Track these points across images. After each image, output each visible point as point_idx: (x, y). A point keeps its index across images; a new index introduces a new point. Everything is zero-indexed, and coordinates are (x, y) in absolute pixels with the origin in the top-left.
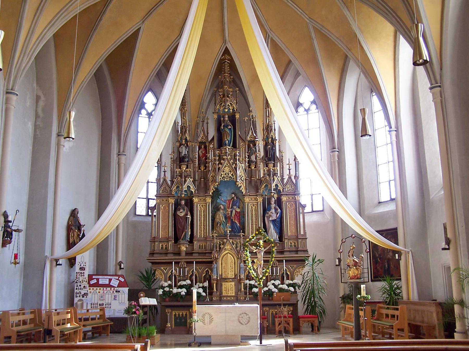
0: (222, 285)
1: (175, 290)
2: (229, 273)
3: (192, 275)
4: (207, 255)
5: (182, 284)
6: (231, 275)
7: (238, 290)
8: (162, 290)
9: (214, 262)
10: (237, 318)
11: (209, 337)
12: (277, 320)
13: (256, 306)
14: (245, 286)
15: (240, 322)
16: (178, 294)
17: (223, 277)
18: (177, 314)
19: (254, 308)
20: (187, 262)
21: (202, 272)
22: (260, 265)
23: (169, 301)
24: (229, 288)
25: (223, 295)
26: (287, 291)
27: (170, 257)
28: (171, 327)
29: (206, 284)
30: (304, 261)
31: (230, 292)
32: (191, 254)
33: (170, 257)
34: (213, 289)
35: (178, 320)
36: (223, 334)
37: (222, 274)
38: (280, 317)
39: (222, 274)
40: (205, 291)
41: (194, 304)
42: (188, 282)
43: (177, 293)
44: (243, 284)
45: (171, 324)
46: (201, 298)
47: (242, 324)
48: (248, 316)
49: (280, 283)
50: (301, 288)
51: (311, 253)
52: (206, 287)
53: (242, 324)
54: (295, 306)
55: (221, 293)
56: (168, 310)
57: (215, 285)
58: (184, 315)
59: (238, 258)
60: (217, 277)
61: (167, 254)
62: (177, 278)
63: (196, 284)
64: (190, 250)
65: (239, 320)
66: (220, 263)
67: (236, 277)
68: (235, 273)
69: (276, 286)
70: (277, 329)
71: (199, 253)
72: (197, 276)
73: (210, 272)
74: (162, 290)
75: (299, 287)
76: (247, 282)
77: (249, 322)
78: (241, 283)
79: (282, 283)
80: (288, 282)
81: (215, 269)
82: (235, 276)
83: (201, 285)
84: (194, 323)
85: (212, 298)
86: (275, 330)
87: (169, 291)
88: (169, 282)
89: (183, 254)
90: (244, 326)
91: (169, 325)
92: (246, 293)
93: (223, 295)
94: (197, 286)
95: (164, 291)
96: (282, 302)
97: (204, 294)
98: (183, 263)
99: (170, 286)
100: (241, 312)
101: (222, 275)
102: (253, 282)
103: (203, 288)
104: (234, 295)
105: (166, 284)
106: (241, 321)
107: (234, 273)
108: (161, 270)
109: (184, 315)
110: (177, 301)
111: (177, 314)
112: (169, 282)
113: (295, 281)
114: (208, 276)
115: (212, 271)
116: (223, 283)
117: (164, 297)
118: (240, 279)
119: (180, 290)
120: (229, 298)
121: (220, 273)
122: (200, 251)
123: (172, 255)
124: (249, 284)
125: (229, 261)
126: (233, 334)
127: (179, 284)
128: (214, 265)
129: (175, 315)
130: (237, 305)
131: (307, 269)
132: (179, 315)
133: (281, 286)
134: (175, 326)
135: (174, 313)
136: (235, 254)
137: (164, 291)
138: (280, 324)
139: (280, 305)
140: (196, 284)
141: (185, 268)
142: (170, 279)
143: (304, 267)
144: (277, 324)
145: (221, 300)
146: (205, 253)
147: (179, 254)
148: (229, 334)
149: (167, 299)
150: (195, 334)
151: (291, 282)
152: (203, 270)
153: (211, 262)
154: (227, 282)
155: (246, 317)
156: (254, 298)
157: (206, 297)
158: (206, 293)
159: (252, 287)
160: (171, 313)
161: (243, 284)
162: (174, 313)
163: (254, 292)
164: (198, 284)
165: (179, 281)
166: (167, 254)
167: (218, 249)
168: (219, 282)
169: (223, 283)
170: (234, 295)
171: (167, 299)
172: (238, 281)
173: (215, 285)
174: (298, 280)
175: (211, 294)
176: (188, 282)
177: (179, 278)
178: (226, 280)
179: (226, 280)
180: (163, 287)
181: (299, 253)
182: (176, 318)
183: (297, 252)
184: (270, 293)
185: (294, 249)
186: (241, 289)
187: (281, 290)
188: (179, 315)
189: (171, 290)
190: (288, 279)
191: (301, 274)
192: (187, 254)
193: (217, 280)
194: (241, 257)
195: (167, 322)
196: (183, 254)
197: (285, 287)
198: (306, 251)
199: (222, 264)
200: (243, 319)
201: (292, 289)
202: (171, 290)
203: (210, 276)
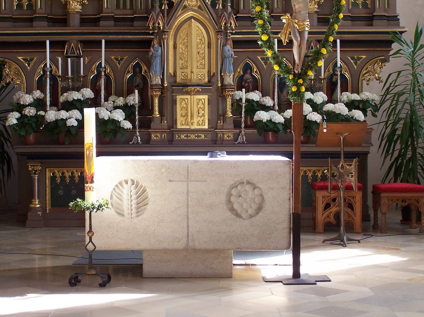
0: (174, 102)
1: (52, 115)
2: (194, 70)
3: (98, 77)
4: (136, 23)
5: (70, 99)
6: (199, 73)
7: (217, 115)
8: (17, 115)
9: (155, 42)
10: (223, 198)
11: (140, 252)
12: (321, 197)
13: (276, 161)
14: (237, 104)
15: (232, 210)
16: (60, 124)
17: (178, 80)
18: (58, 175)
19: (271, 167)
20: (86, 44)
21: (124, 71)
22: (301, 33)
23: (37, 142)
24: (194, 112)
25: (179, 126)
26: (348, 119)
27: (40, 28)
28: (43, 208)
29: (134, 99)
30: (389, 43)
31: (195, 120)
32: (95, 21)
33: (40, 28)
34: (152, 111)
35: (61, 192)
36: (180, 245)
37: (175, 72)
38: (335, 188)
39: (175, 72)
40: (129, 117)
41: (86, 153)
42: (88, 93)
43: (56, 121)
44: (229, 101)
45: (43, 202)
46: (119, 135)
47: (238, 215)
48: (256, 191)
49: (326, 99)
50: (379, 114)
51: (407, 24)
52: (133, 106)
53: (238, 215)
54: (362, 157)
55: (174, 122)
56: (34, 167)
57: (156, 101)
58: (77, 180)
59: (218, 32)
60: (162, 80)
61: (31, 20)
62: (61, 84)
63: (106, 100)
64: (91, 12)
65: (229, 202)
66: (171, 43)
67: (213, 80)
68: (209, 72)
69: (316, 107)
70: (321, 217)
71: (116, 20)
72: (112, 77)
73: (144, 68)
74: (17, 115)
75: (376, 108)
76: (242, 95)
77: (259, 209)
78: (224, 99)
79: (332, 100)
80: (347, 96)
81: (158, 60)
82: (211, 77)
83: (120, 101)
84: (87, 213)
85: (149, 135)
86: (314, 219)
87: (36, 116)
88: (38, 94)
89: (75, 21)
90: (246, 222)
91: (36, 204)
92: (237, 125)
93: (179, 126)
94: (110, 104)
95: (23, 116)
96: (341, 149)
97: (127, 125)
98: (73, 42)
99: (39, 104)
100: (238, 179)
101: (175, 75)
102: (255, 96)
103: (128, 110)
104: (206, 127)
105: (28, 99)
106: (236, 206)
107: (206, 71)
108: (18, 62)
109: (77, 180)
110: (58, 142)
111: (58, 175)
112: (38, 94)
113: (366, 95)
114: (138, 80)
115: (149, 65)
116: (179, 97)
117: (23, 133)
118: (224, 87)
119: (63, 114)
120: (193, 137)
121: (171, 71)
122: (119, 13)
123: (45, 23)
124: (247, 100)
125: (195, 40)
126: (210, 246)
127: (62, 99)
128: (155, 50)
129: (53, 179)
130: (223, 157)
131: (394, 64)
132: (63, 178)
133: (330, 107)
134: (52, 205)
135: (49, 174)
136: (210, 21)
137: (23, 116)
138: (327, 206)
139: (336, 156)
140: (106, 100)
141: (79, 57)
142: (41, 87)
143: (385, 61)
144: (320, 206)
145: (174, 143)
146: (132, 20)
147: (63, 21)
148: (197, 246)
149: (31, 138)
150: (90, 247)
151: (355, 97)
152: (127, 60)
153: (148, 44)
154: (188, 93)
155: (250, 193)
156: (266, 137)
157: (132, 132)
158: (133, 122)
159: (253, 107)
160: (42, 174)
161: (229, 101)
162: (49, 174)
163: (260, 121)
164: (111, 98)
165: (66, 90)
166: (31, 20)
167: (165, 7)
168: (168, 95)
169: (179, 97)
170: (206, 127)
171: (31, 138)
172: (217, 91)
173: (156, 101)
174: (370, 93)
175: (146, 124)
176: (88, 93)
177: (64, 84)
178: (185, 87)
179: (185, 87)
180: (20, 108)
181: (375, 22)
182: (54, 187)
183: (370, 19)
184: (309, 126)
185: (361, 12)
186: (224, 113)
187: (331, 117)
188: (63, 178)
189: (42, 113)
190: (344, 89)
191: (379, 79)
192: (85, 21)
193: (162, 88)
194: (226, 28)
195: (32, 197)
196: (75, 21)
197: (340, 108)
198: (394, 19)
199: (175, 47)
200: (240, 200)
201: (358, 114)
202: (42, 113)
203: (144, 79)
